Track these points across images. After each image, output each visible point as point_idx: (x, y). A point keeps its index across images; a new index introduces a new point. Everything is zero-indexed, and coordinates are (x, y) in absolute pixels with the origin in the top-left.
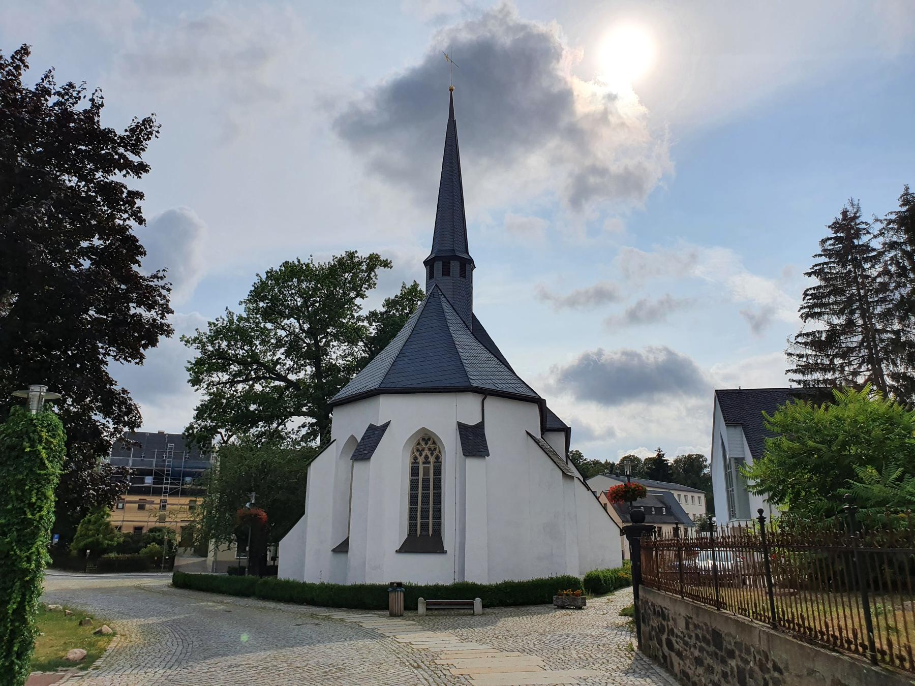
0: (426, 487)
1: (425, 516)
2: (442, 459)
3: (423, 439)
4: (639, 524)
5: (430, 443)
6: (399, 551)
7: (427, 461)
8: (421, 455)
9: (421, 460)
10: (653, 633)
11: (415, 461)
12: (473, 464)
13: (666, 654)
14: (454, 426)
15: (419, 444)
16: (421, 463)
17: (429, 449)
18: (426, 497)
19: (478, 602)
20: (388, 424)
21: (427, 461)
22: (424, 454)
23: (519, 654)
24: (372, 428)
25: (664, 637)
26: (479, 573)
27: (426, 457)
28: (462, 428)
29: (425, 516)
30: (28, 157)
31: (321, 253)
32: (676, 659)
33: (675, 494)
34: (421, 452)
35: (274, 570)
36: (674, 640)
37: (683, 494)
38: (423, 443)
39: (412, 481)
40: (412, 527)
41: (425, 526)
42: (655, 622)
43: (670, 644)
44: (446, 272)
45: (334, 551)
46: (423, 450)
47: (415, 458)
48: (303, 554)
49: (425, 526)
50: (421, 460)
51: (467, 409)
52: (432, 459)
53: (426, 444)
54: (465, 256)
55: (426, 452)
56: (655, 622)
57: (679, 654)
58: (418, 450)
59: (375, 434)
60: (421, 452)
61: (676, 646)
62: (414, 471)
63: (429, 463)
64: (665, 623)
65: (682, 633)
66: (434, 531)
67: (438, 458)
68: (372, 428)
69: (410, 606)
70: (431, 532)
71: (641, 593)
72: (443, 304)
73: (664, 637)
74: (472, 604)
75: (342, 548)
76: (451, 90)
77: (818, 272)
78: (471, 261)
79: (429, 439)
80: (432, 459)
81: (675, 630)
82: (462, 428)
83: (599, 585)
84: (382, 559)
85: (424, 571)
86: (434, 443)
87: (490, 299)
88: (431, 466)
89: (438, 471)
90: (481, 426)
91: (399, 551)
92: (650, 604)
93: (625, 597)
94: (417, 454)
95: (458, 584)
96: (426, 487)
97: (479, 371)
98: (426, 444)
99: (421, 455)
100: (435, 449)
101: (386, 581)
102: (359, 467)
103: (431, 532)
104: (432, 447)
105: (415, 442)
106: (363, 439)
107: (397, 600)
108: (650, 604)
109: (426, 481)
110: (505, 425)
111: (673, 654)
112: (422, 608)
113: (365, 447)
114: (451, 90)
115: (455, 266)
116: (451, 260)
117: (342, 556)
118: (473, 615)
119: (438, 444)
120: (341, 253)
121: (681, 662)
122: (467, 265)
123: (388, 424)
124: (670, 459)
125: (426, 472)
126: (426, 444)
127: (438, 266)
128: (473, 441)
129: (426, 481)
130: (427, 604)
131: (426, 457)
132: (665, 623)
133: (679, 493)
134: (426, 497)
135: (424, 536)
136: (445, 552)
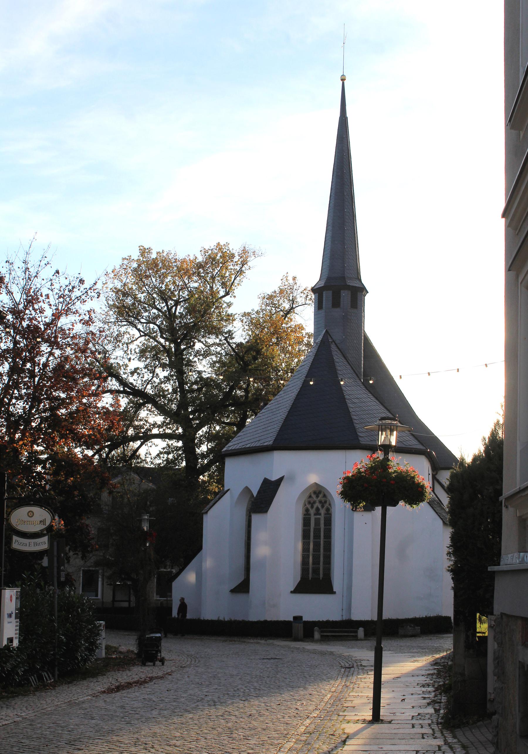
0: (317, 536)
2: (332, 510)
3: (315, 493)
6: (294, 592)
7: (317, 512)
9: (312, 512)
11: (307, 513)
15: (310, 497)
17: (320, 502)
19: (361, 632)
21: (317, 512)
22: (315, 506)
24: (266, 483)
27: (318, 509)
31: (188, 248)
34: (312, 504)
38: (314, 496)
39: (325, 639)
44: (336, 303)
45: (233, 591)
47: (307, 510)
48: (202, 584)
49: (316, 571)
50: (312, 512)
52: (323, 511)
53: (317, 497)
58: (309, 503)
59: (269, 489)
60: (312, 504)
62: (306, 522)
63: (320, 514)
66: (324, 574)
67: (328, 510)
68: (266, 483)
70: (321, 576)
72: (334, 353)
74: (356, 632)
75: (243, 587)
76: (343, 80)
79: (320, 492)
80: (323, 511)
84: (278, 596)
85: (317, 608)
86: (325, 496)
87: (381, 325)
89: (328, 522)
91: (294, 592)
94: (309, 506)
96: (317, 536)
98: (317, 497)
100: (326, 502)
103: (321, 576)
105: (308, 494)
106: (259, 492)
109: (317, 531)
112: (317, 635)
114: (343, 80)
115: (345, 296)
116: (341, 289)
117: (240, 597)
119: (329, 497)
120: (210, 244)
122: (359, 292)
125: (317, 521)
126: (316, 501)
127: (327, 295)
129: (317, 531)
131: (318, 509)
135: (315, 578)
136: (335, 593)
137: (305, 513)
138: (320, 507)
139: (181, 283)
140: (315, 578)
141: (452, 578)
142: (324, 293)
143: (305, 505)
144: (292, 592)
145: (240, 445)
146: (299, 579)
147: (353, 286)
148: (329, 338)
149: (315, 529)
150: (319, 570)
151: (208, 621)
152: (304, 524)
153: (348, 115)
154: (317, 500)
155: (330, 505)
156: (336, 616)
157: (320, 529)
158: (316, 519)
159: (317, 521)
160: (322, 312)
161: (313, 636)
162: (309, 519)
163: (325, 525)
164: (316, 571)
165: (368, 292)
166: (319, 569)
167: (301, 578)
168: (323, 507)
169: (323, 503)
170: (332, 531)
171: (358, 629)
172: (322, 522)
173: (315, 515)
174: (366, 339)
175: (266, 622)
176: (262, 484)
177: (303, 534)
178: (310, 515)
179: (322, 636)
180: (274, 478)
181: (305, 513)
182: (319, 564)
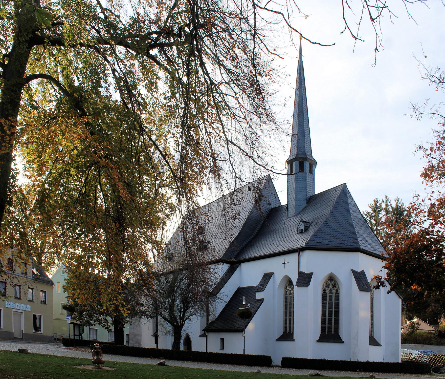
0: (330, 307)
1: (330, 323)
7: (331, 292)
9: (328, 291)
11: (324, 292)
15: (286, 288)
16: (328, 293)
18: (330, 321)
21: (331, 292)
29: (330, 323)
30: (59, 190)
41: (330, 329)
44: (301, 168)
47: (324, 290)
49: (330, 329)
50: (328, 291)
62: (324, 298)
63: (332, 293)
67: (337, 290)
76: (341, 33)
77: (376, 208)
80: (334, 292)
83: (157, 342)
89: (337, 297)
91: (200, 336)
95: (407, 361)
96: (330, 307)
103: (333, 333)
105: (284, 287)
109: (331, 304)
114: (334, 44)
115: (307, 165)
125: (331, 297)
131: (331, 290)
134: (330, 321)
139: (83, 239)
142: (294, 163)
144: (277, 340)
145: (314, 244)
151: (145, 349)
159: (331, 297)
160: (293, 177)
169: (334, 286)
173: (329, 293)
175: (237, 354)
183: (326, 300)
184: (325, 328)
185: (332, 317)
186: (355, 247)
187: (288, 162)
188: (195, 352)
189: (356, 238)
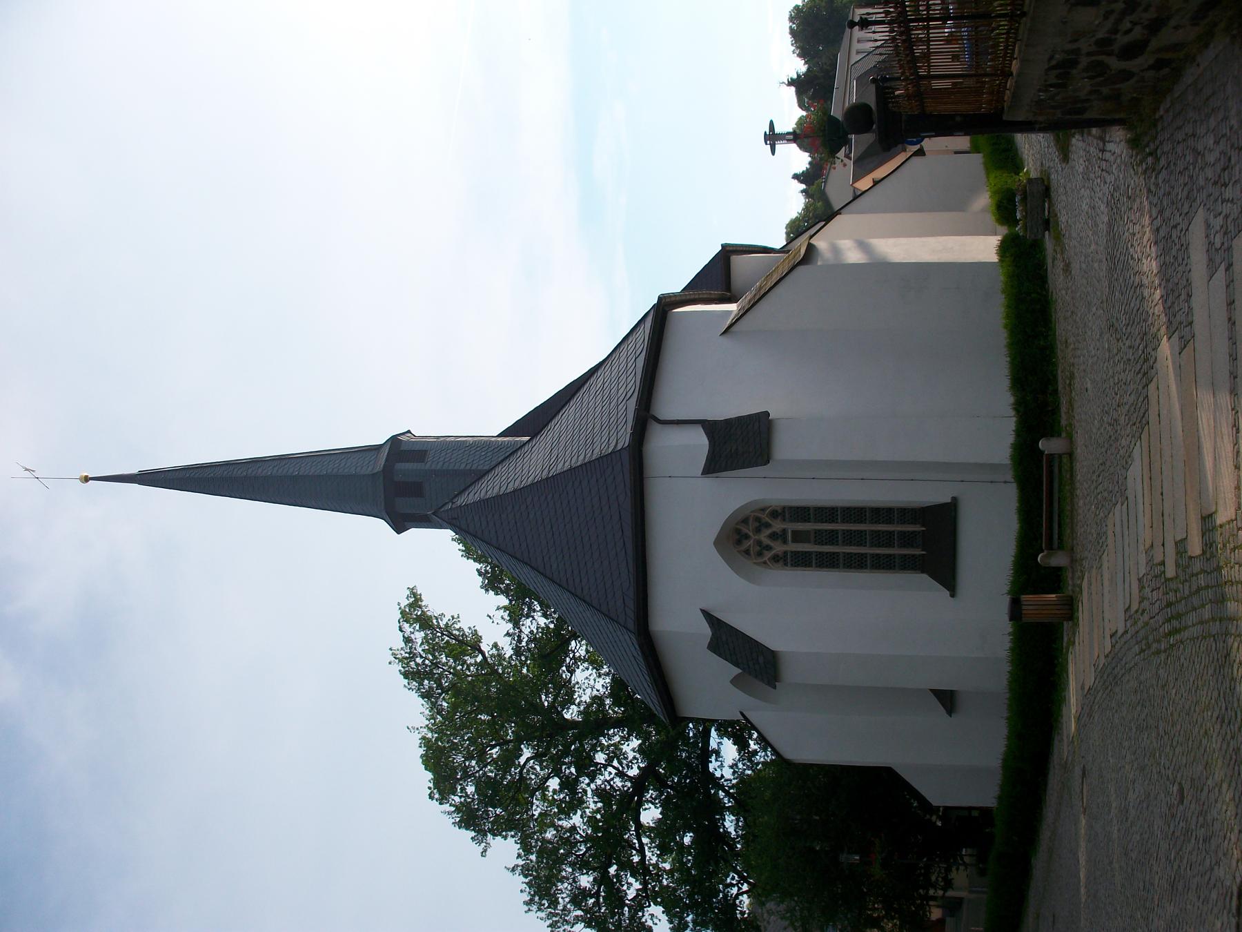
0: (831, 538)
3: (739, 542)
4: (875, 116)
5: (745, 530)
7: (780, 536)
8: (769, 548)
9: (779, 548)
10: (1105, 90)
11: (783, 560)
12: (785, 447)
13: (1151, 62)
14: (710, 483)
15: (747, 552)
17: (758, 530)
18: (850, 538)
20: (707, 615)
21: (780, 536)
22: (766, 541)
23: (1152, 387)
24: (716, 646)
25: (1114, 63)
26: (991, 433)
27: (773, 536)
28: (714, 466)
31: (410, 714)
32: (1167, 36)
33: (855, 58)
34: (763, 548)
35: (985, 812)
36: (1122, 40)
37: (856, 46)
38: (747, 544)
39: (1057, 542)
40: (908, 565)
42: (1082, 85)
43: (1131, 51)
46: (759, 543)
47: (776, 559)
48: (955, 765)
49: (907, 539)
50: (779, 548)
51: (678, 452)
52: (778, 526)
53: (747, 537)
54: (386, 451)
55: (763, 537)
56: (1082, 85)
57: (1155, 27)
58: (760, 554)
59: (727, 641)
60: (763, 548)
61: (1138, 33)
62: (801, 561)
63: (784, 531)
64: (1084, 61)
65: (1106, 17)
67: (775, 514)
68: (716, 646)
69: (1052, 580)
71: (1021, 116)
73: (1114, 63)
75: (947, 699)
78: (394, 440)
79: (738, 531)
80: (778, 526)
81: (1100, 35)
82: (714, 466)
84: (959, 626)
85: (989, 539)
86: (745, 521)
88: (792, 527)
89: (800, 513)
90: (713, 428)
92: (1043, 96)
93: (1033, 149)
94: (768, 555)
96: (831, 538)
97: (600, 431)
98: (747, 537)
99: (769, 548)
100: (758, 519)
101: (1007, 626)
102: (790, 673)
104: (753, 525)
106: (737, 665)
107: (1040, 603)
108: (1043, 96)
109: (821, 537)
110: (714, 382)
111: (1154, 43)
112: (1058, 560)
113: (755, 662)
114: (86, 479)
116: (399, 482)
118: (1071, 455)
121: (1173, 23)
123: (707, 615)
124: (798, 66)
125: (798, 537)
126: (748, 539)
127: (405, 505)
128: (739, 443)
129: (821, 537)
130: (1050, 547)
131: (773, 536)
132: (1084, 61)
133: (853, 52)
134: (850, 538)
135: (919, 541)
136: (954, 499)
137: (781, 562)
138: (769, 532)
140: (919, 541)
141: (792, 32)
143: (765, 563)
144: (953, 596)
146: (925, 576)
147: (387, 460)
148: (446, 508)
149: (816, 543)
150: (905, 532)
152: (806, 566)
153: (135, 471)
154: (754, 537)
155: (763, 510)
156: (1007, 498)
157: (816, 532)
158: (795, 540)
159: (798, 537)
161: (1059, 569)
162: (796, 554)
163: (806, 519)
164: (907, 539)
165: (409, 432)
166: (902, 534)
167: (923, 572)
168: (768, 526)
169: (761, 526)
170: (819, 505)
171: (1042, 453)
172: (801, 526)
173: (785, 542)
174: (506, 433)
176: (720, 655)
177: (827, 567)
178: (785, 553)
179: (1061, 547)
180: (706, 631)
181: (781, 562)
182: (891, 533)
183: (810, 553)
184: (849, 556)
185: (836, 531)
186: (993, 318)
187: (399, 528)
188: (1000, 798)
189: (600, 458)
